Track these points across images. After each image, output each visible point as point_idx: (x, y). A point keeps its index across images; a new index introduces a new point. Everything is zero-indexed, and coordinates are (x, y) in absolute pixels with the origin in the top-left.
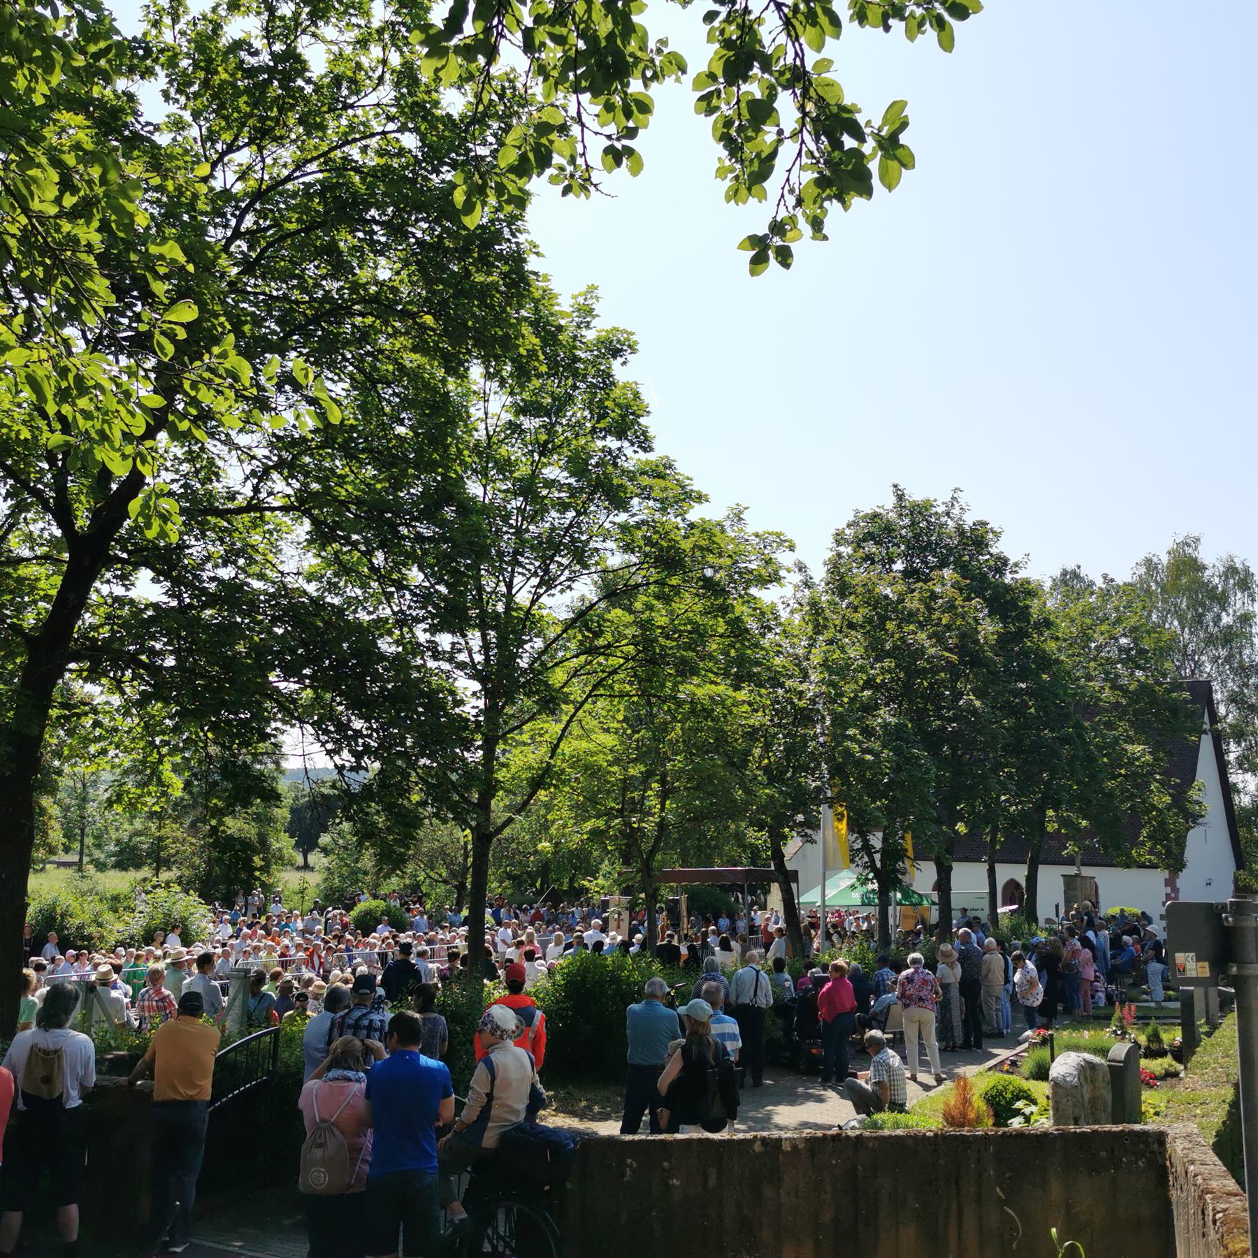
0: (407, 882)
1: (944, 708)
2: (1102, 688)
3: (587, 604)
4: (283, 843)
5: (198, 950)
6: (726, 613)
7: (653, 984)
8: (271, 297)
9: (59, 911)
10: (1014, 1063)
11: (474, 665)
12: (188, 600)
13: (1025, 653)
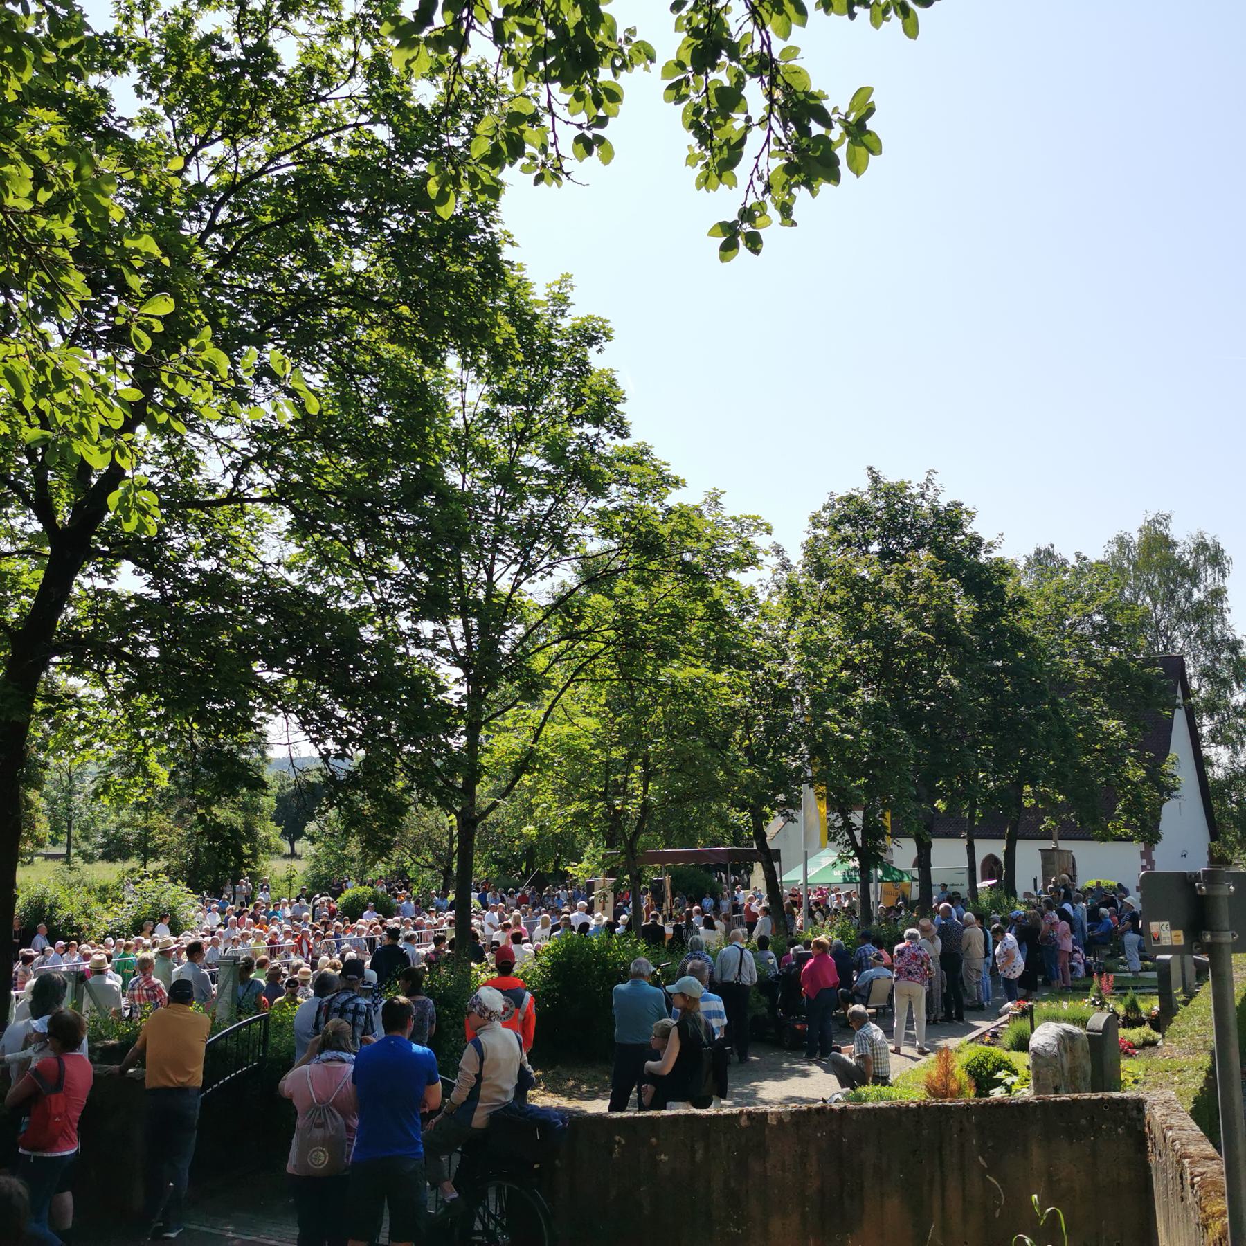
0: (394, 868)
3: (568, 590)
4: (270, 831)
5: (188, 939)
8: (247, 289)
9: (47, 902)
10: (995, 1035)
12: (170, 592)
13: (1000, 631)
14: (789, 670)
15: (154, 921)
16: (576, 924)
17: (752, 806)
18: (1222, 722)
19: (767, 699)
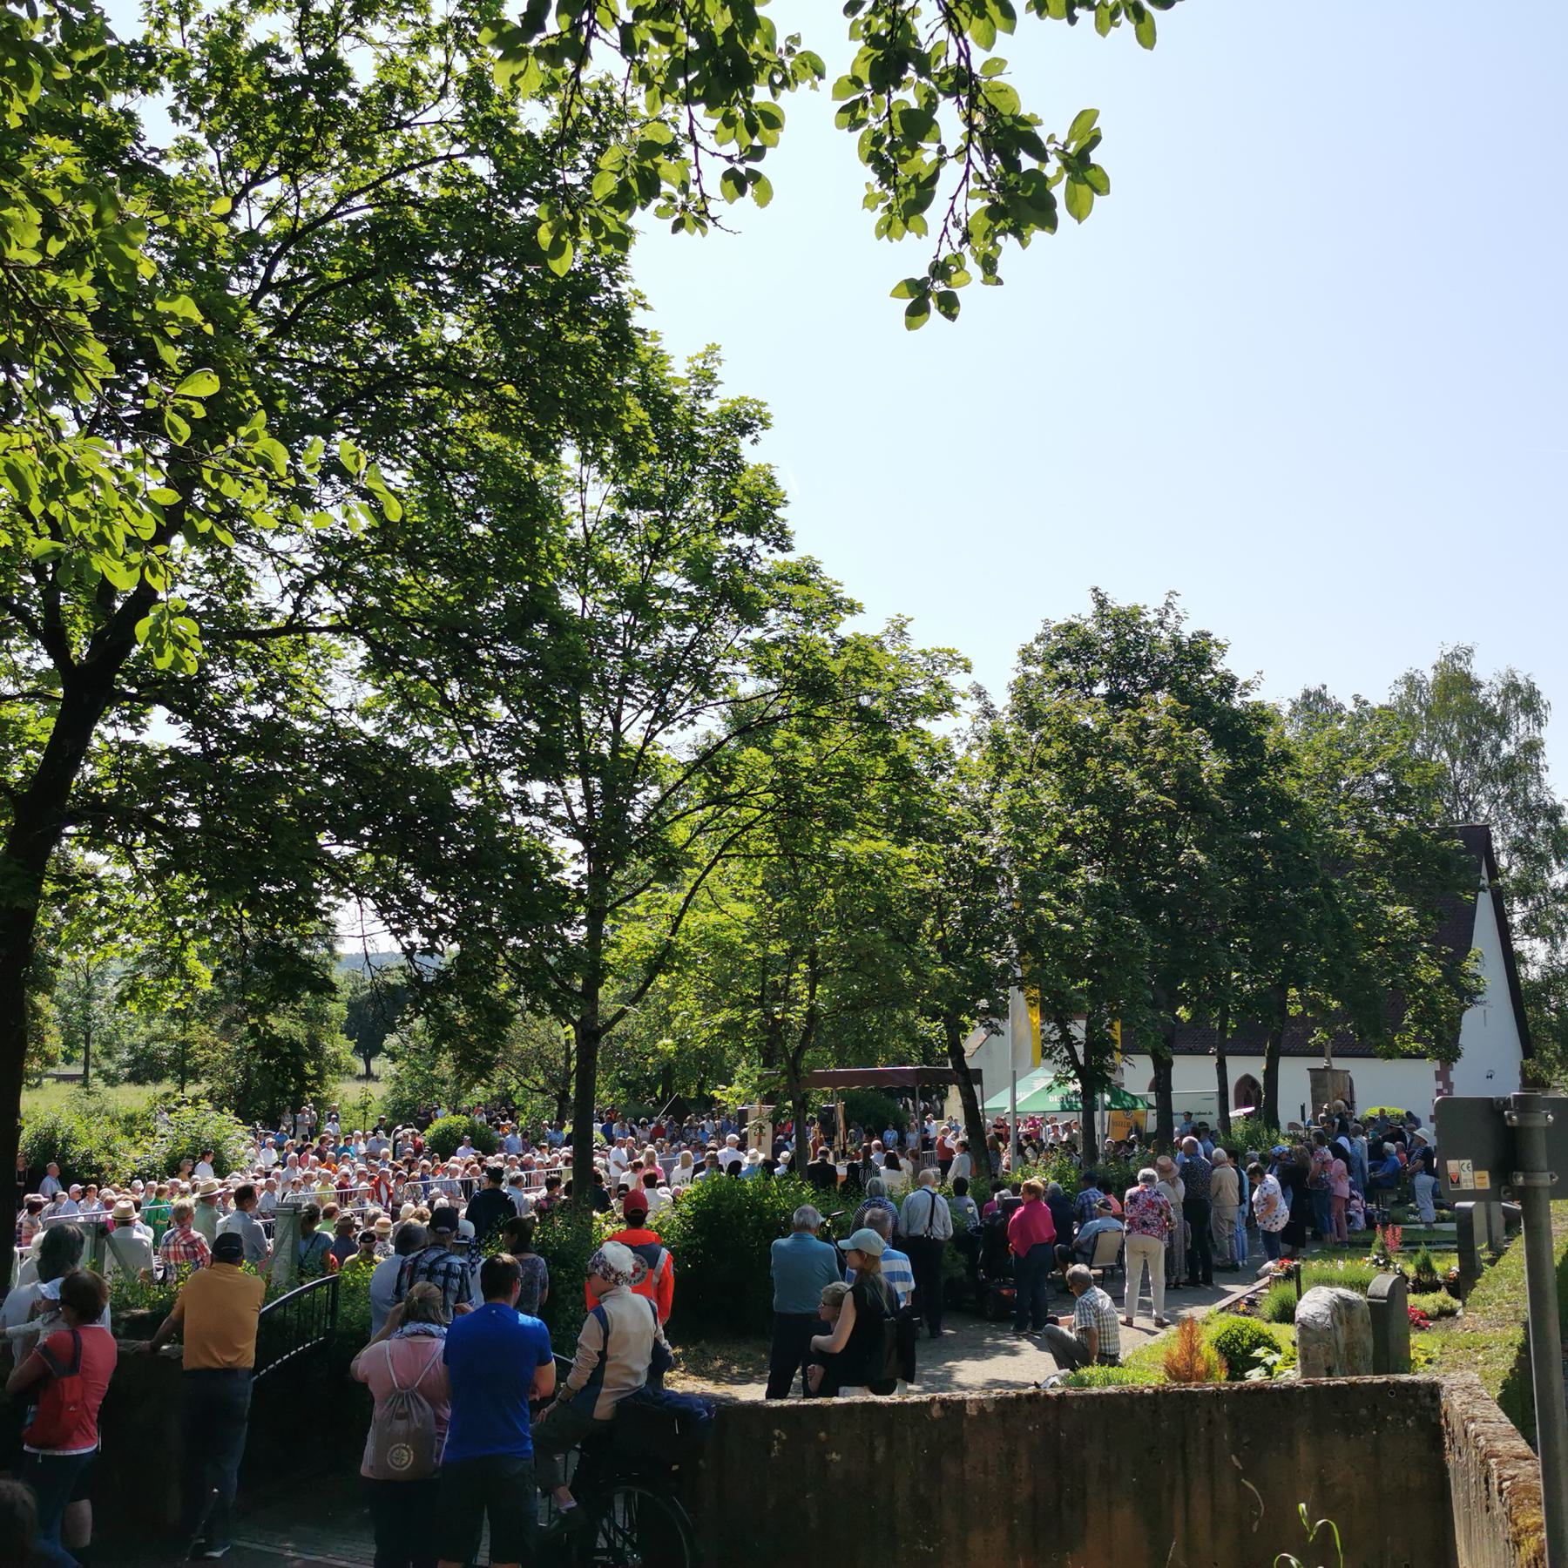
0: (496, 1092)
2: (1355, 836)
3: (715, 742)
4: (340, 1046)
5: (236, 1181)
8: (311, 364)
9: (59, 1135)
10: (1252, 1303)
11: (574, 821)
12: (214, 745)
13: (1259, 794)
14: (993, 843)
15: (194, 1158)
16: (725, 1163)
17: (946, 1015)
18: (1538, 908)
19: (965, 880)
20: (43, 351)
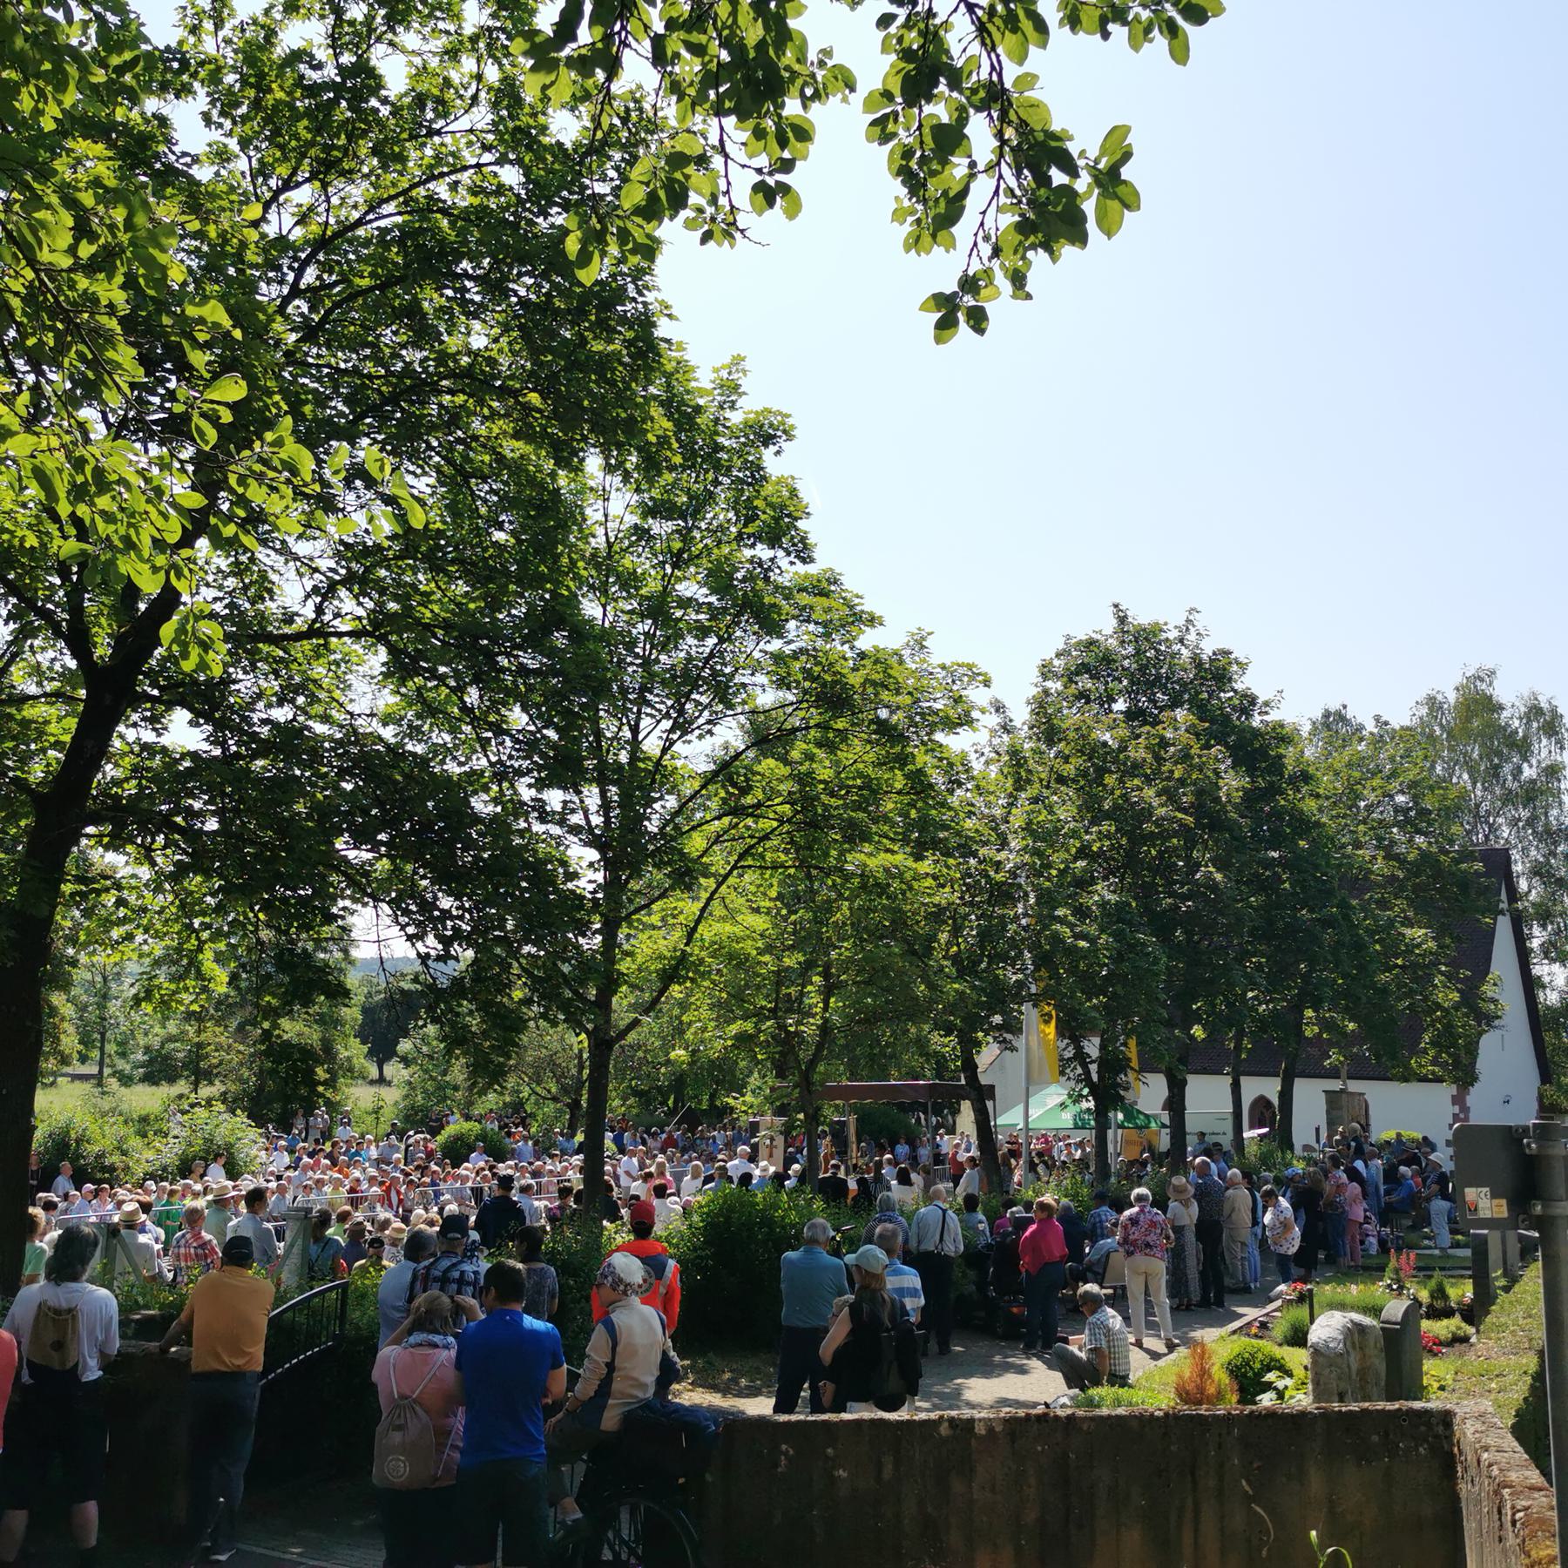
0: (508, 1099)
1: (1176, 882)
2: (1374, 857)
3: (732, 753)
4: (353, 1050)
5: (247, 1184)
6: (905, 764)
7: (814, 1226)
8: (338, 370)
9: (73, 1136)
10: (1263, 1326)
11: (591, 829)
12: (234, 748)
13: (1277, 814)
20: (72, 354)
